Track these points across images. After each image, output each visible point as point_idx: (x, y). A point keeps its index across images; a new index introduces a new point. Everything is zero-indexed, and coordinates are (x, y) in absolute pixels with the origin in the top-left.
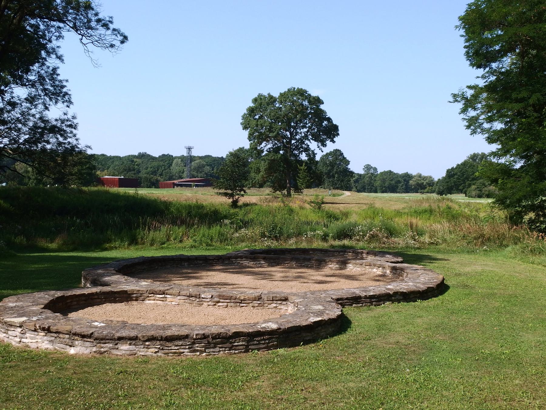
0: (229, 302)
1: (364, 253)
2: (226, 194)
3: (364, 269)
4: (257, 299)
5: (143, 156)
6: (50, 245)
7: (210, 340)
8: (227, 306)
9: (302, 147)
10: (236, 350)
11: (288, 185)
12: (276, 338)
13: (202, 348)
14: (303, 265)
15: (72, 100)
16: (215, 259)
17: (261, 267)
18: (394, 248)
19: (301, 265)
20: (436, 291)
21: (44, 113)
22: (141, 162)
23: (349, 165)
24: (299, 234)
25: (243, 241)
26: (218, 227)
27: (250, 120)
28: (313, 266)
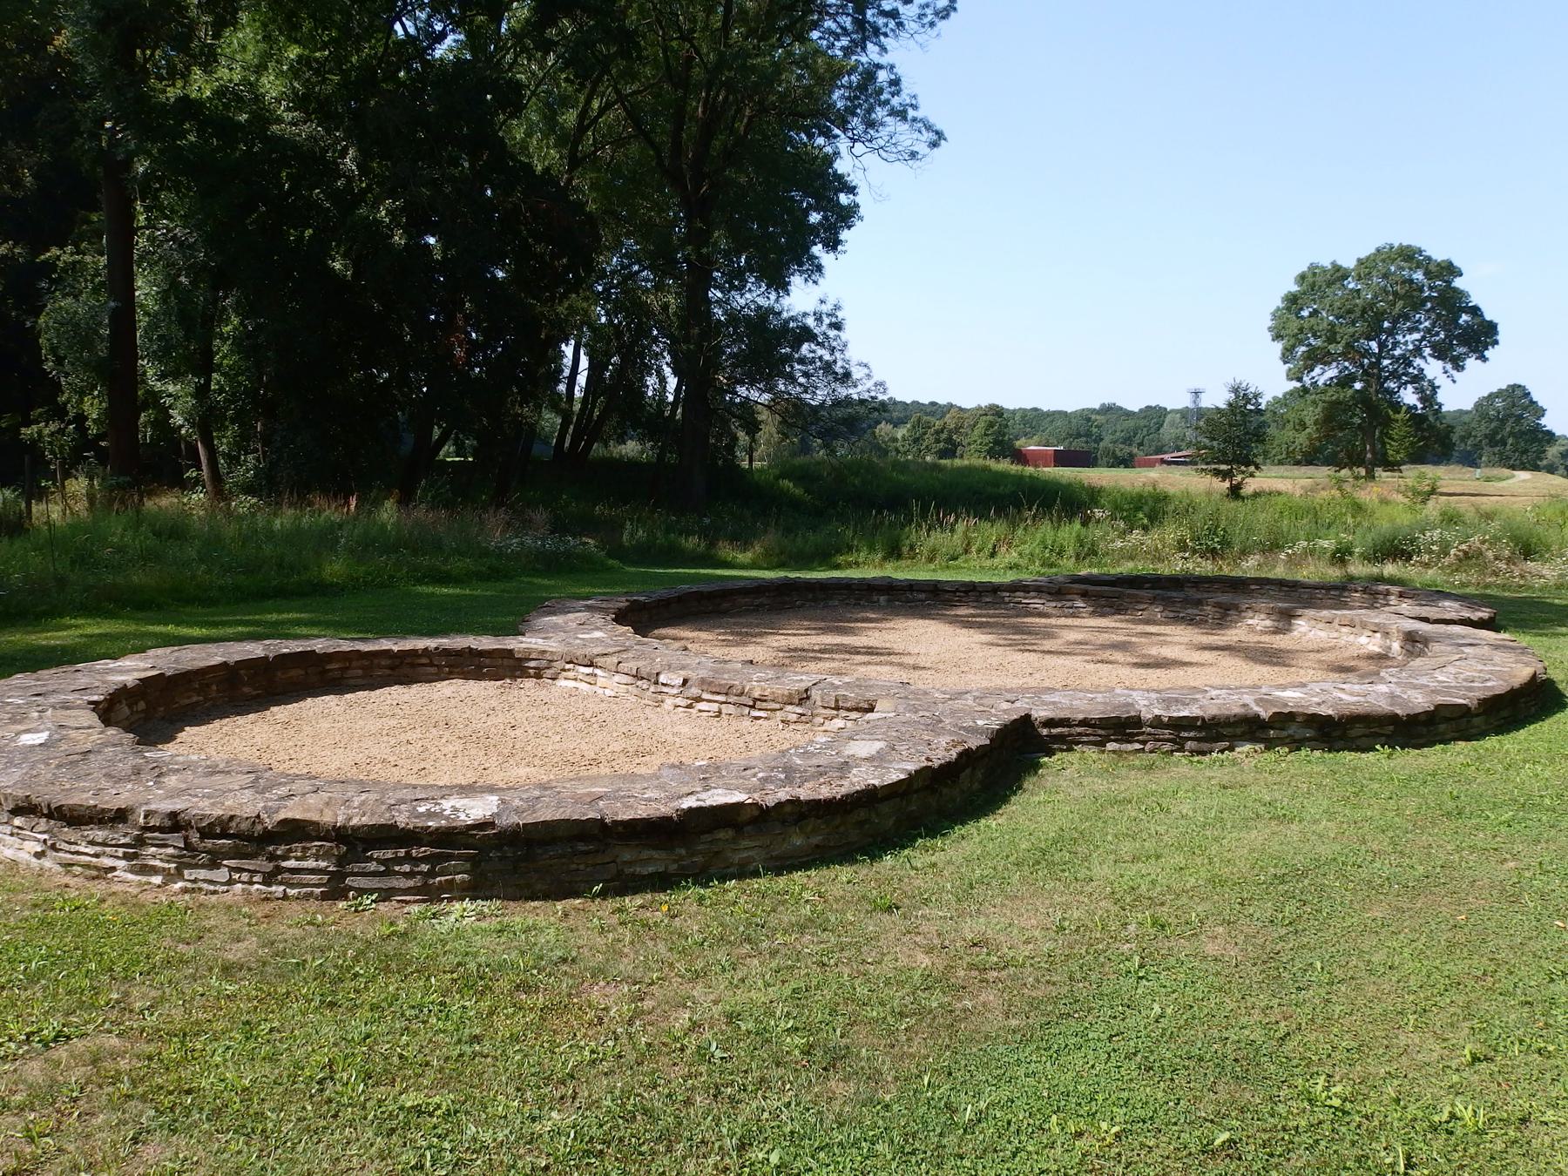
1: (1392, 594)
2: (1217, 473)
5: (1108, 410)
7: (195, 838)
8: (720, 712)
10: (292, 886)
11: (1369, 456)
12: (467, 858)
13: (168, 862)
14: (1181, 615)
16: (957, 590)
17: (1073, 616)
18: (1521, 586)
19: (1176, 615)
20: (1476, 721)
22: (1104, 421)
23: (1543, 419)
24: (1273, 546)
25: (1132, 558)
26: (1077, 526)
27: (1288, 319)
28: (1207, 621)
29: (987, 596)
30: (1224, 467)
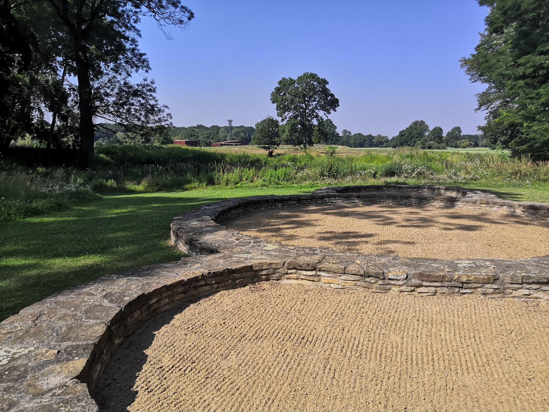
0: (440, 287)
2: (264, 148)
3: (479, 207)
4: (492, 281)
5: (200, 127)
6: (137, 187)
8: (436, 292)
9: (313, 115)
11: (304, 141)
15: (150, 66)
16: (308, 199)
21: (127, 80)
29: (319, 200)
30: (267, 146)
